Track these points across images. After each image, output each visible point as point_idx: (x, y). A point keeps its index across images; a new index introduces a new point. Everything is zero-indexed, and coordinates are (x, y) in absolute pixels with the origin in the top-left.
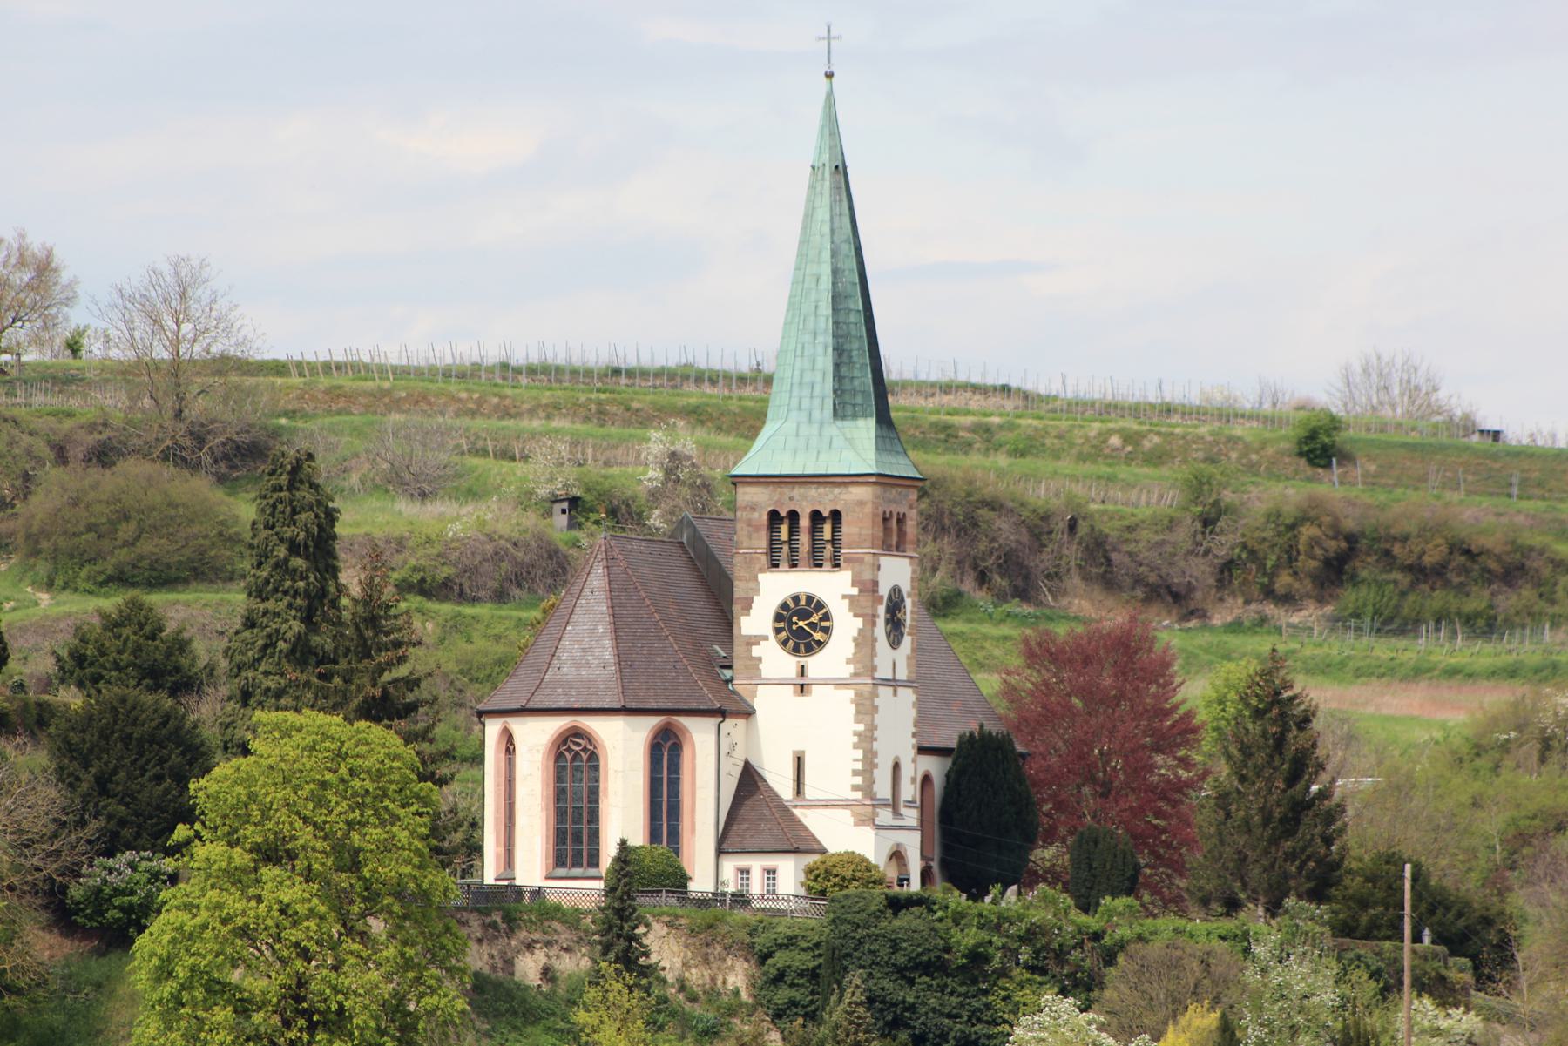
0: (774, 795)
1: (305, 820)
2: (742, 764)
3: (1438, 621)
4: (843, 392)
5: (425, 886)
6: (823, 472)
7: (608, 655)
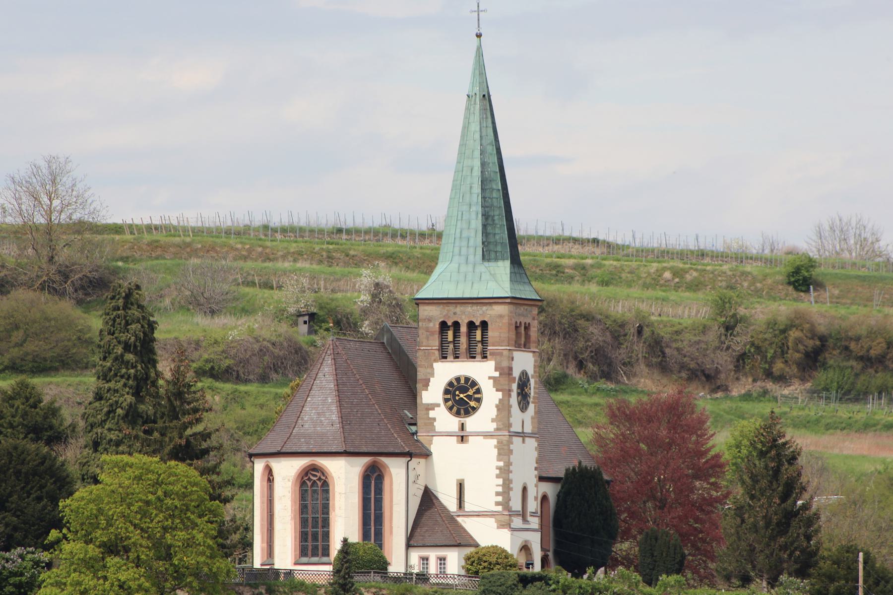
0: (445, 508)
1: (135, 526)
2: (423, 488)
3: (880, 393)
4: (489, 243)
5: (214, 570)
6: (475, 296)
7: (335, 417)
